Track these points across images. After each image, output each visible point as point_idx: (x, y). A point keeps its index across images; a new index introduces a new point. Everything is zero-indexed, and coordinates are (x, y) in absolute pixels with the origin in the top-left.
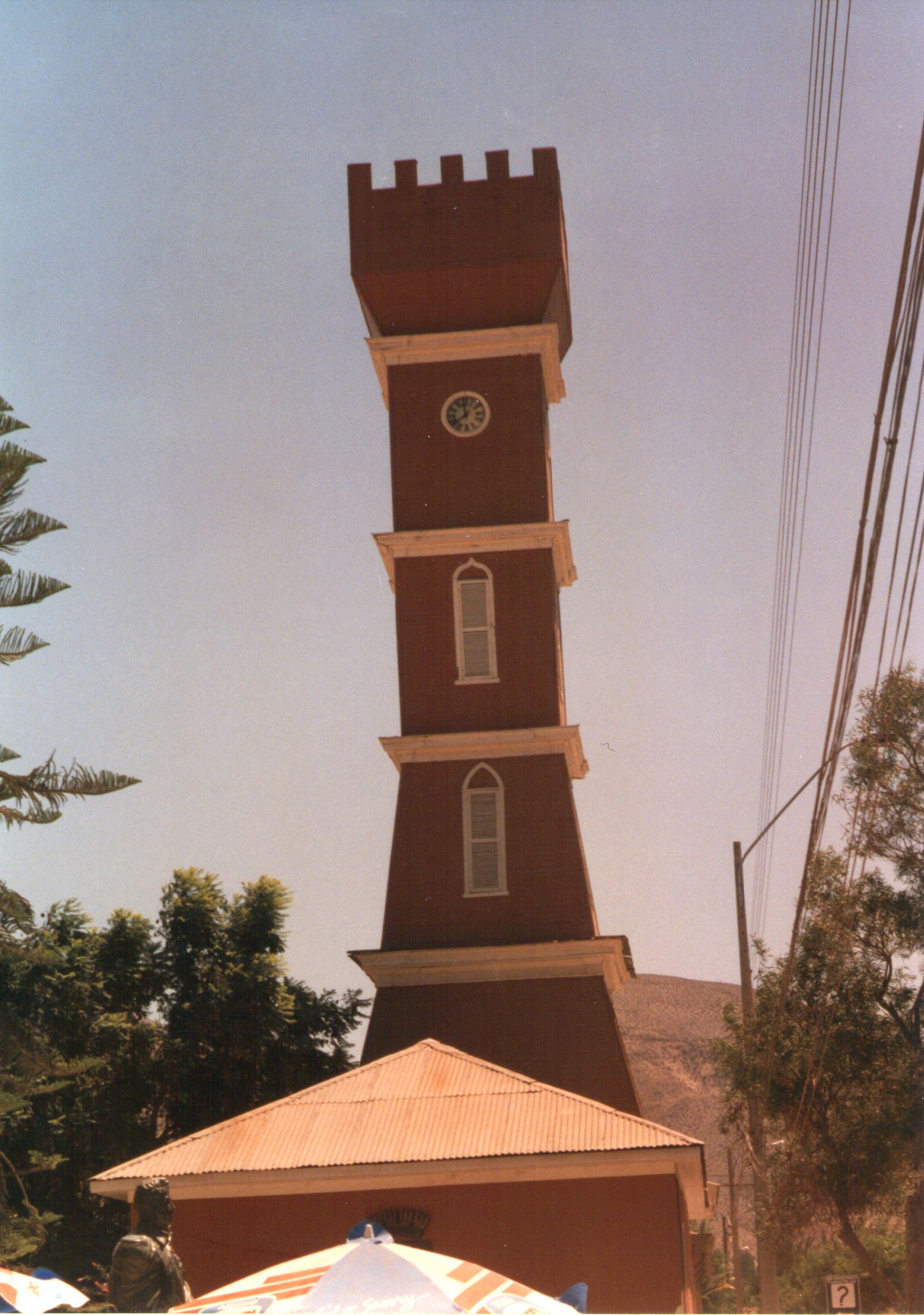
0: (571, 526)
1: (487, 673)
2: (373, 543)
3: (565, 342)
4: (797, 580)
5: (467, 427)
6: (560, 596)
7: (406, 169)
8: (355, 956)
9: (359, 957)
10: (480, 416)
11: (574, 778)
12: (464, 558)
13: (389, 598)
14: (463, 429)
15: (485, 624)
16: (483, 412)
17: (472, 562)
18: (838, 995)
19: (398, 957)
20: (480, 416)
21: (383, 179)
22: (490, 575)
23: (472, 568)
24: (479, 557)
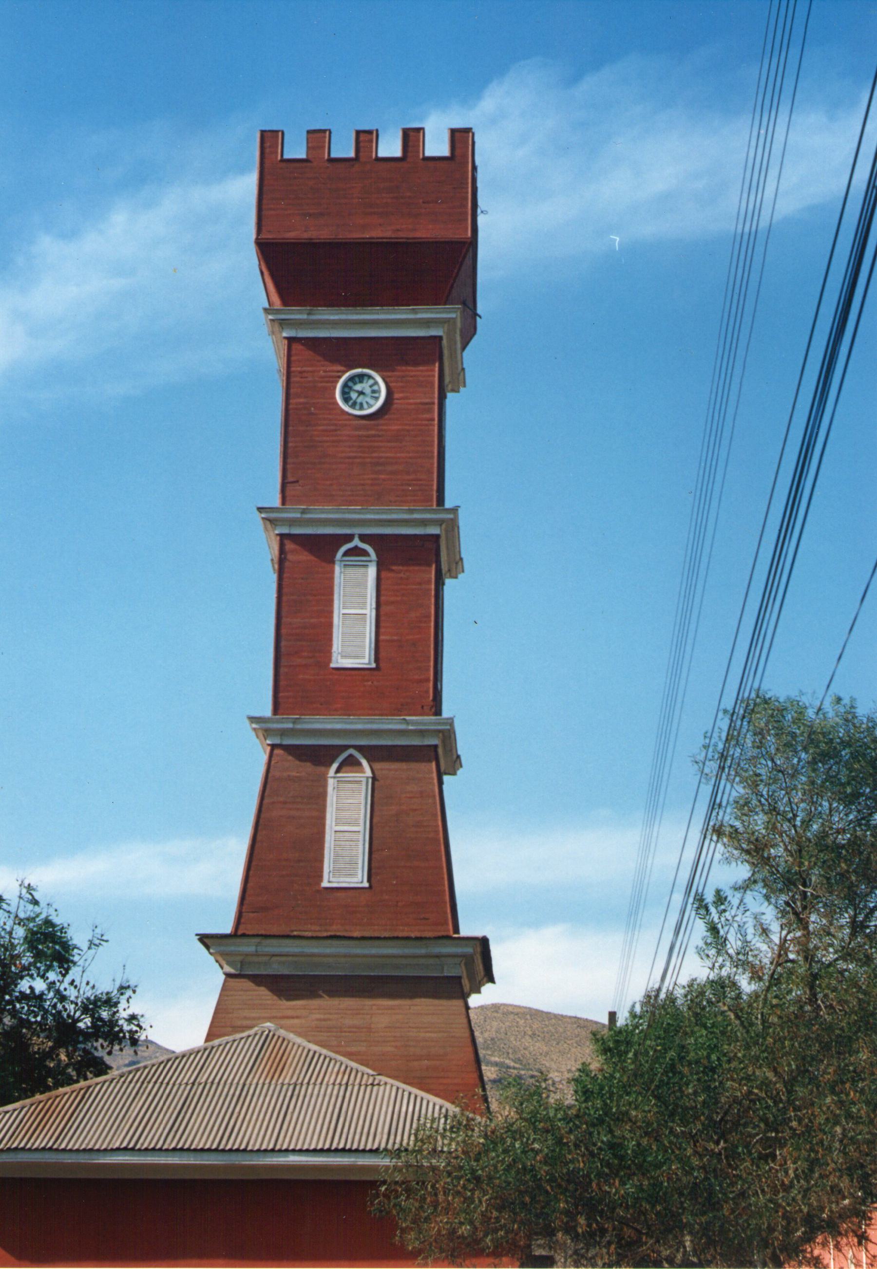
0: (461, 513)
1: (364, 657)
2: (496, 979)
3: (469, 332)
4: (677, 734)
5: (361, 404)
6: (445, 587)
7: (318, 138)
8: (205, 939)
9: (206, 940)
10: (376, 395)
11: (446, 774)
12: (349, 538)
13: (271, 579)
14: (358, 407)
15: (364, 608)
16: (379, 391)
17: (356, 542)
18: (617, 1175)
19: (247, 947)
20: (376, 395)
21: (295, 149)
22: (373, 556)
23: (356, 547)
24: (363, 538)
